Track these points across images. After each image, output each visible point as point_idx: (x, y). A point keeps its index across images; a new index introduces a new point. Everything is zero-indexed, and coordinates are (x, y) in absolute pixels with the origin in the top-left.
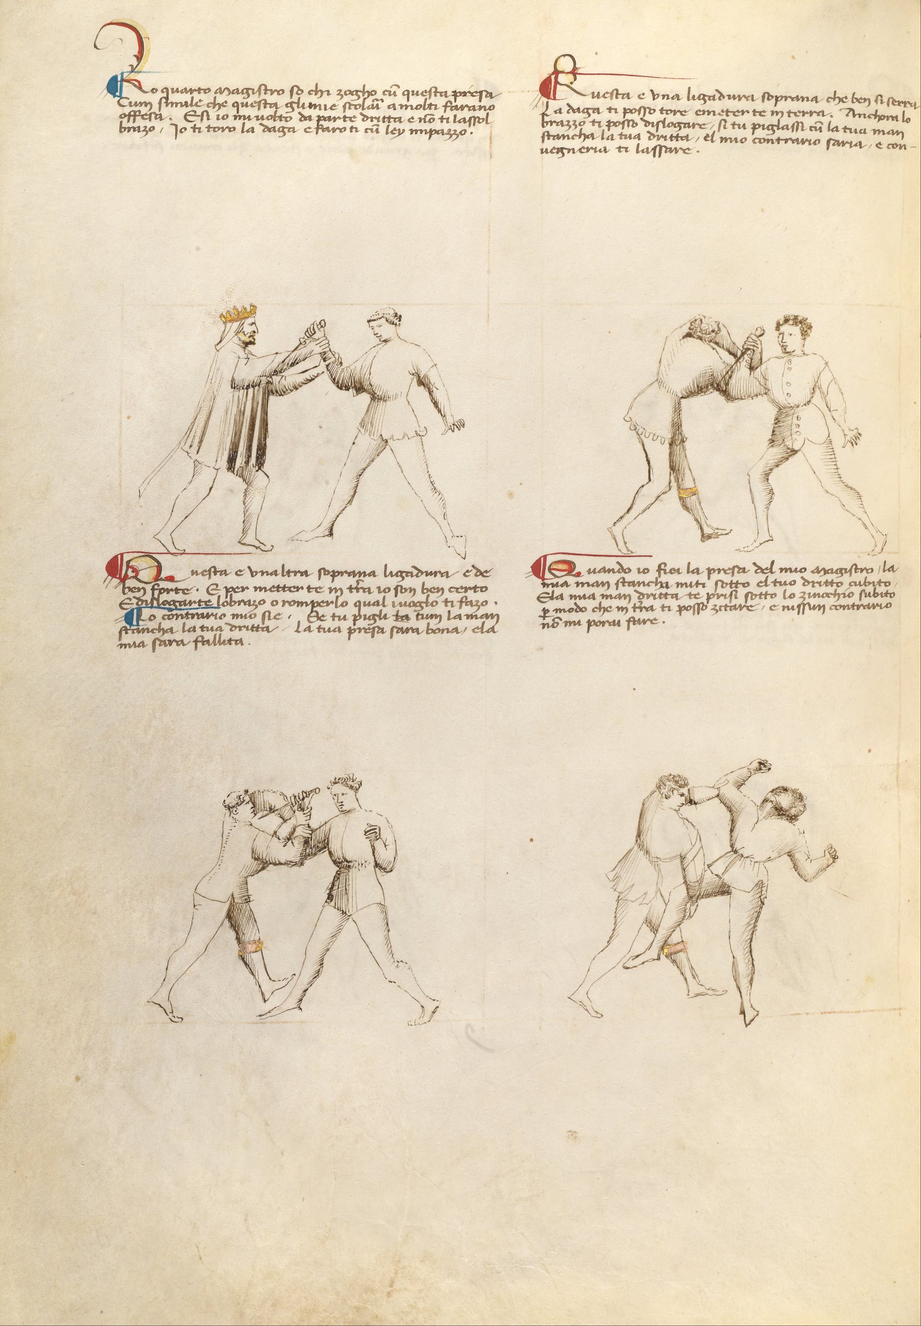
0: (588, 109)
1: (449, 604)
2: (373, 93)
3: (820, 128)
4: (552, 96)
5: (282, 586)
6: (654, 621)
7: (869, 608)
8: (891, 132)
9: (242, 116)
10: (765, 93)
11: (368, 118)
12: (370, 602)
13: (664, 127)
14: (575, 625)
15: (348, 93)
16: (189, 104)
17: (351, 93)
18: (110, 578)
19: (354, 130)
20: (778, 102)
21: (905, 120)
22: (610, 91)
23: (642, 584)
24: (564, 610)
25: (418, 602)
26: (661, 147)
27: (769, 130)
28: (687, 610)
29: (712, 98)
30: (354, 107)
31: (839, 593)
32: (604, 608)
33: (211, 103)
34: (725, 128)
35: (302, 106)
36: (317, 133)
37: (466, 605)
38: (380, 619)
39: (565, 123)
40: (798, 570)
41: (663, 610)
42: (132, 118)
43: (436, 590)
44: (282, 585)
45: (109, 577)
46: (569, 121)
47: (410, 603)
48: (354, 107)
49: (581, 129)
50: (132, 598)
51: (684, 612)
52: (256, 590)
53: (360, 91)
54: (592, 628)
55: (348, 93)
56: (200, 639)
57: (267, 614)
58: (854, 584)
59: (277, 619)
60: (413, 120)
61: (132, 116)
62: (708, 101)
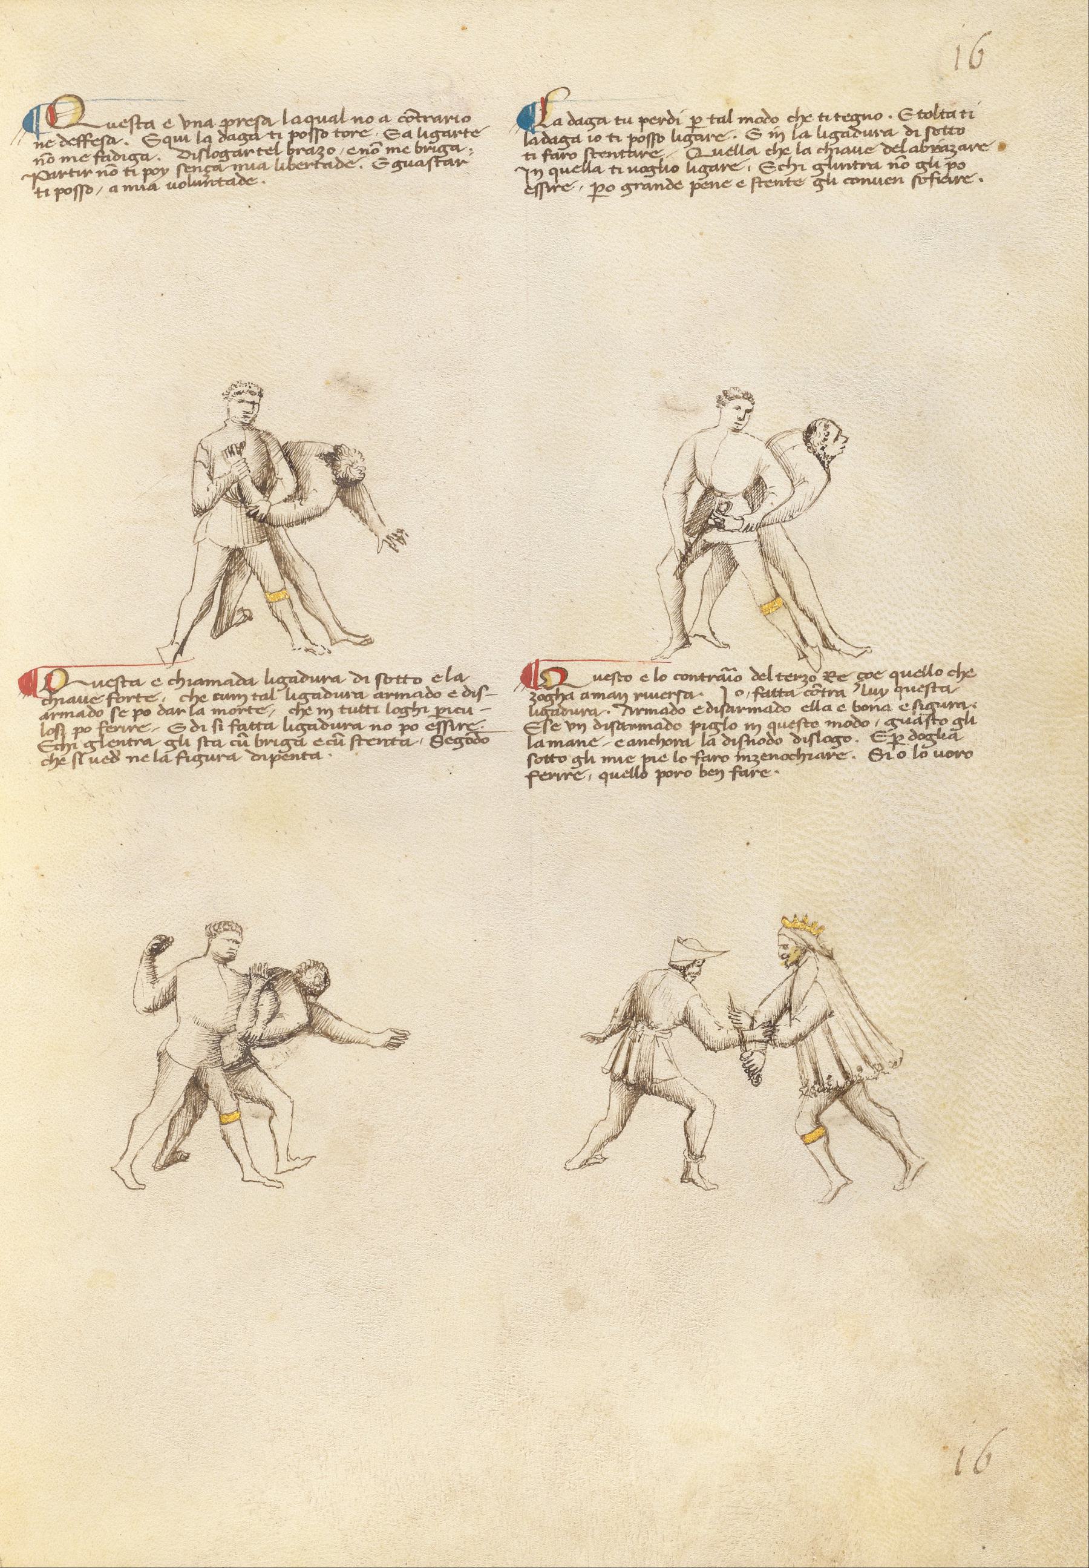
0: (135, 155)
1: (276, 137)
2: (437, 695)
3: (341, 741)
4: (532, 685)
5: (257, 723)
6: (364, 134)
7: (173, 714)
8: (820, 755)
9: (939, 756)
10: (259, 117)
11: (198, 727)
12: (600, 676)
13: (818, 741)
14: (696, 680)
15: (779, 741)
16: (338, 118)
17: (831, 740)
18: (522, 686)
19: (616, 171)
20: (275, 763)
21: (678, 759)
22: (128, 119)
23: (97, 683)
24: (656, 710)
25: (835, 737)
26: (82, 187)
27: (298, 730)
28: (66, 194)
29: (144, 157)
30: (783, 678)
31: (803, 754)
32: (196, 696)
33: (294, 709)
34: (81, 763)
35: (970, 721)
36: (178, 763)
37: (552, 158)
38: (661, 172)
39: (752, 758)
40: (659, 695)
41: (613, 173)
42: (82, 144)
43: (893, 181)
44: (778, 689)
45: (522, 684)
46: (756, 756)
47: (641, 168)
48: (347, 711)
49: (258, 735)
50: (688, 757)
51: (62, 196)
52: (741, 122)
53: (657, 168)
54: (664, 780)
55: (779, 741)
56: (760, 690)
57: (218, 723)
58: (332, 743)
59: (662, 761)
60: (159, 683)
61: (236, 725)
62: (694, 141)
